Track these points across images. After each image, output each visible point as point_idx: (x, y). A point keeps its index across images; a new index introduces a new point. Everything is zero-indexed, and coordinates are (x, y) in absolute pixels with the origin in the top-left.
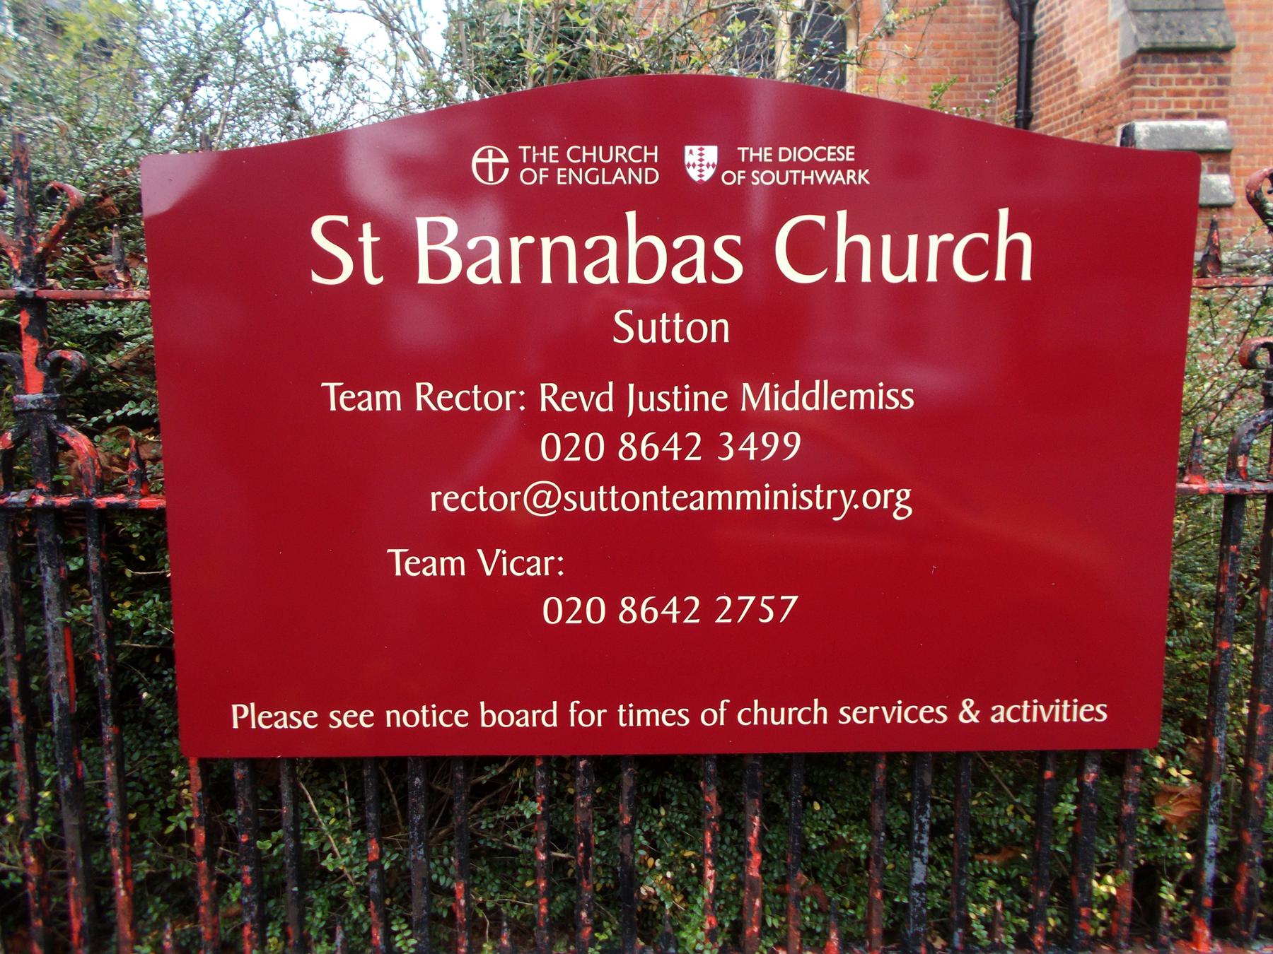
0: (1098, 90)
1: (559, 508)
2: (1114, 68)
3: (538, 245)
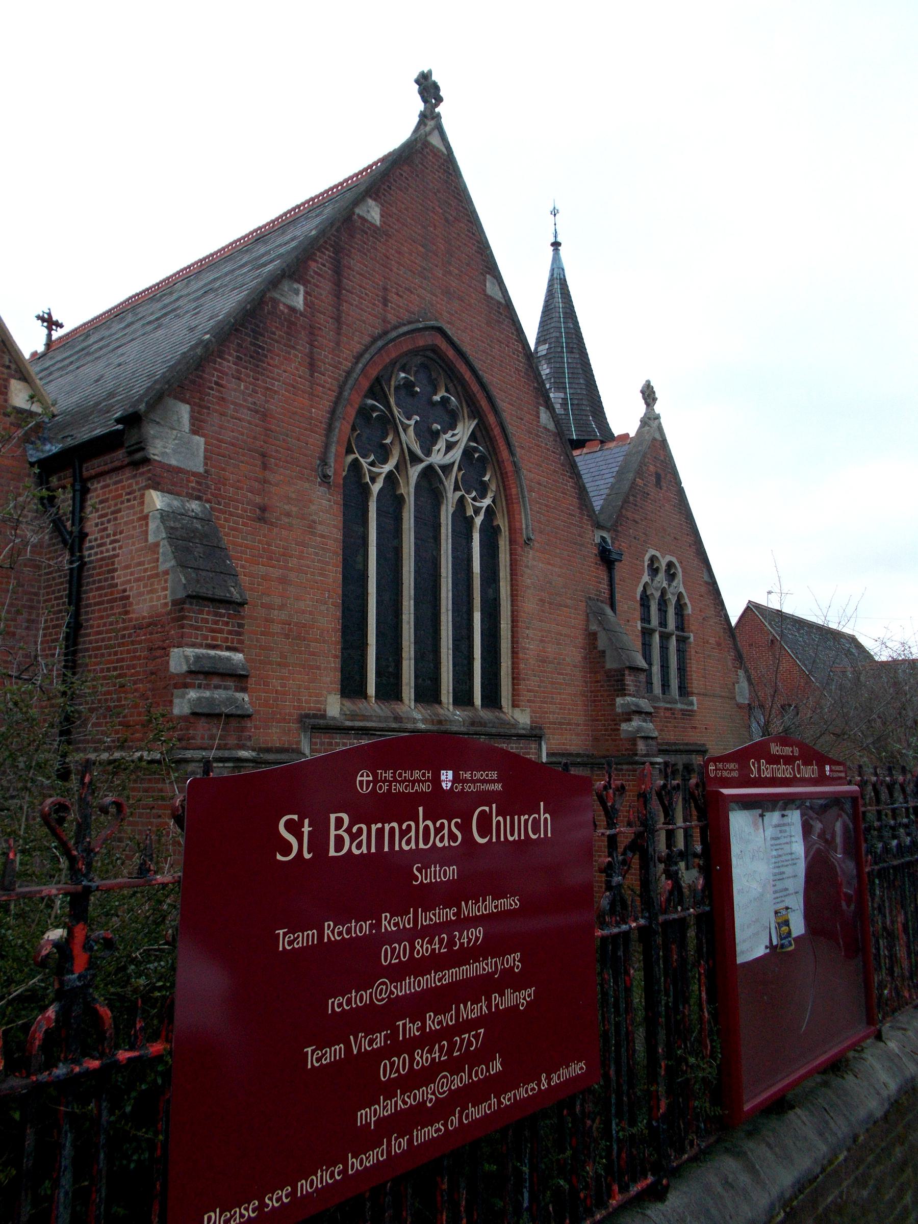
0: (151, 617)
1: (389, 997)
2: (166, 604)
3: (383, 828)
